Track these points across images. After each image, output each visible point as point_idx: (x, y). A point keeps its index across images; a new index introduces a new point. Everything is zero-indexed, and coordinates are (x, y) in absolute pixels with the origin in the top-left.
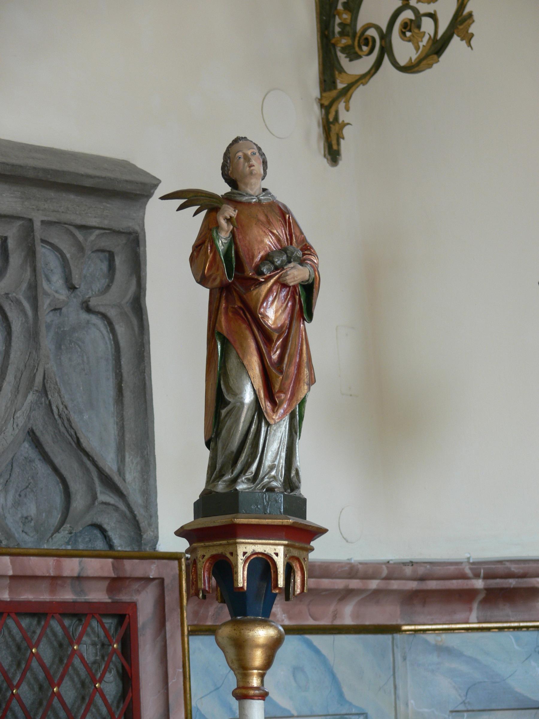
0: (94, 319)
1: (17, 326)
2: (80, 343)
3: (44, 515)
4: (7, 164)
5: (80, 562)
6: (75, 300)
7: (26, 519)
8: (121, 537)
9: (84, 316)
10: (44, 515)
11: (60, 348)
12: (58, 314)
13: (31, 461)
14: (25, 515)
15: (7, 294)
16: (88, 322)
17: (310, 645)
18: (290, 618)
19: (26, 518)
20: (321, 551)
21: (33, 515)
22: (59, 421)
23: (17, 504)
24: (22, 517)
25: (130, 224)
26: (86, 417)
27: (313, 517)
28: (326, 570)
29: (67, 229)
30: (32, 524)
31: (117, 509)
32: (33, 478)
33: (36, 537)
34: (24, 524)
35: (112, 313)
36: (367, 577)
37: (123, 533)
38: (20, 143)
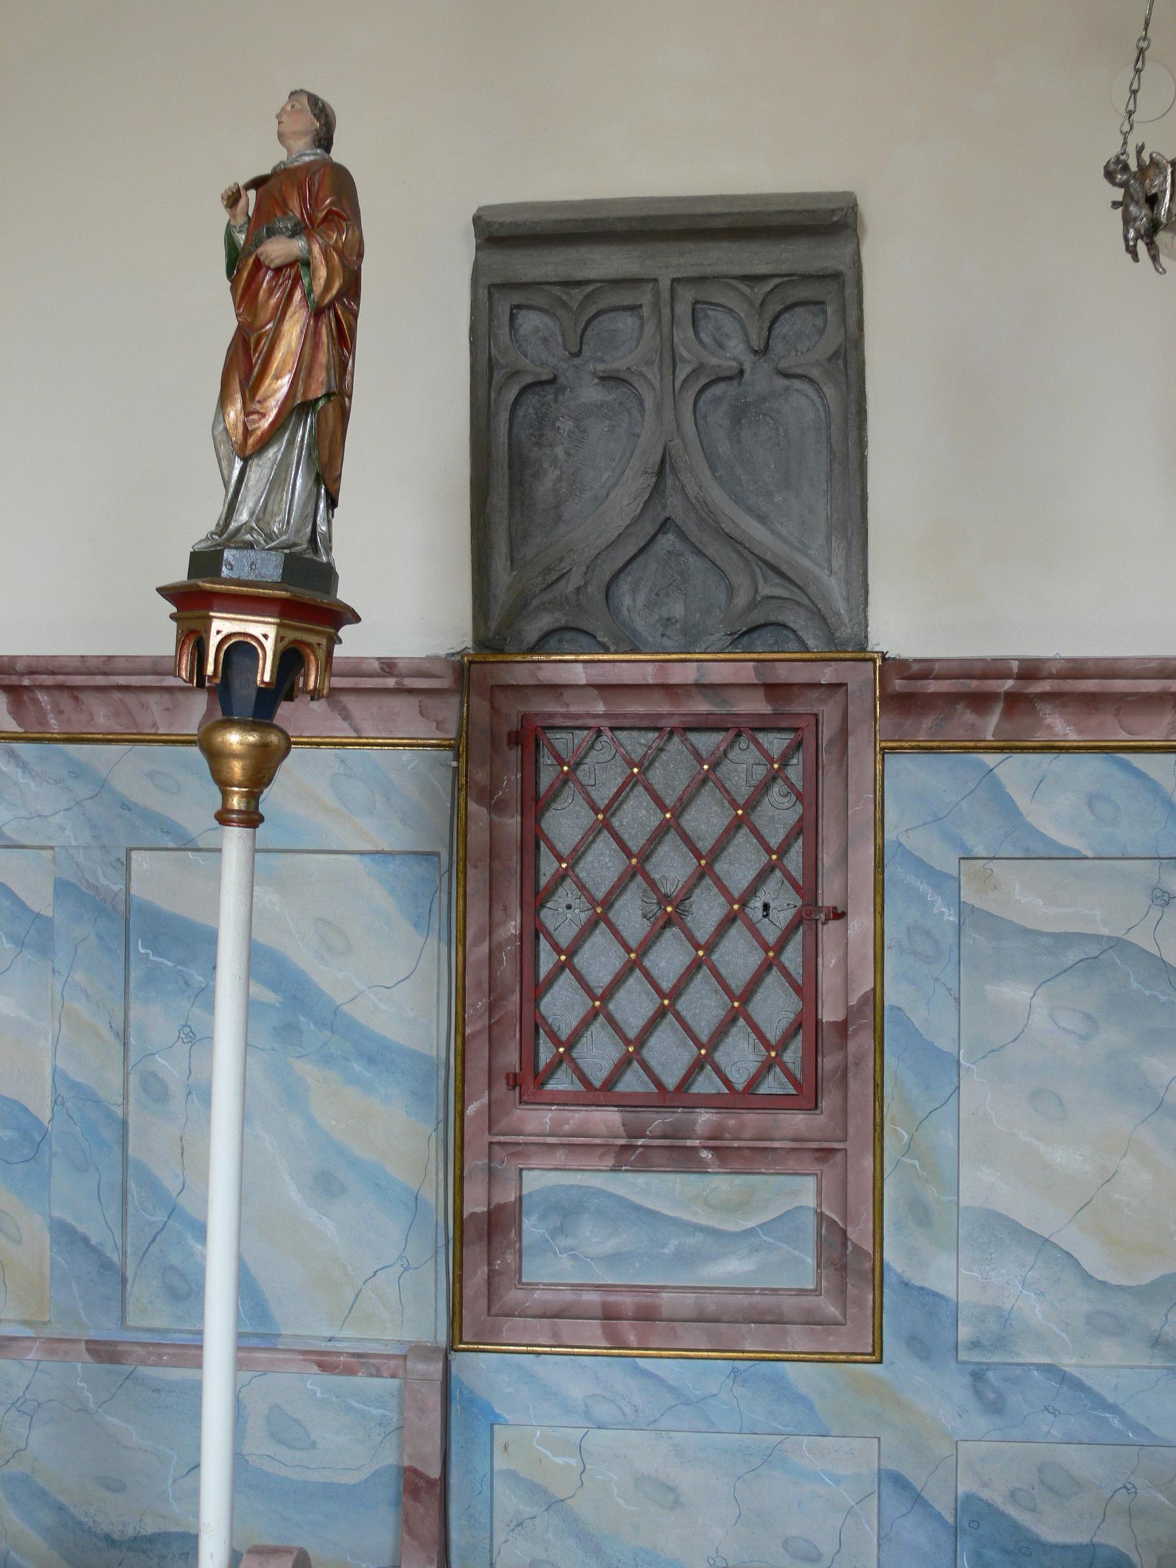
0: (797, 384)
1: (649, 403)
2: (774, 414)
3: (698, 615)
4: (576, 221)
5: (698, 669)
6: (766, 365)
7: (668, 622)
8: (815, 636)
9: (781, 382)
10: (698, 615)
11: (739, 422)
12: (736, 384)
13: (679, 554)
14: (665, 616)
15: (628, 369)
16: (787, 389)
17: (1127, 767)
18: (1080, 732)
19: (668, 620)
20: (352, 644)
21: (678, 616)
22: (698, 506)
23: (650, 605)
24: (661, 619)
25: (828, 264)
26: (778, 498)
27: (345, 593)
28: (356, 669)
29: (729, 284)
30: (678, 626)
31: (799, 604)
32: (681, 573)
33: (683, 641)
34: (666, 626)
35: (815, 373)
36: (925, 675)
37: (817, 632)
38: (643, 198)
